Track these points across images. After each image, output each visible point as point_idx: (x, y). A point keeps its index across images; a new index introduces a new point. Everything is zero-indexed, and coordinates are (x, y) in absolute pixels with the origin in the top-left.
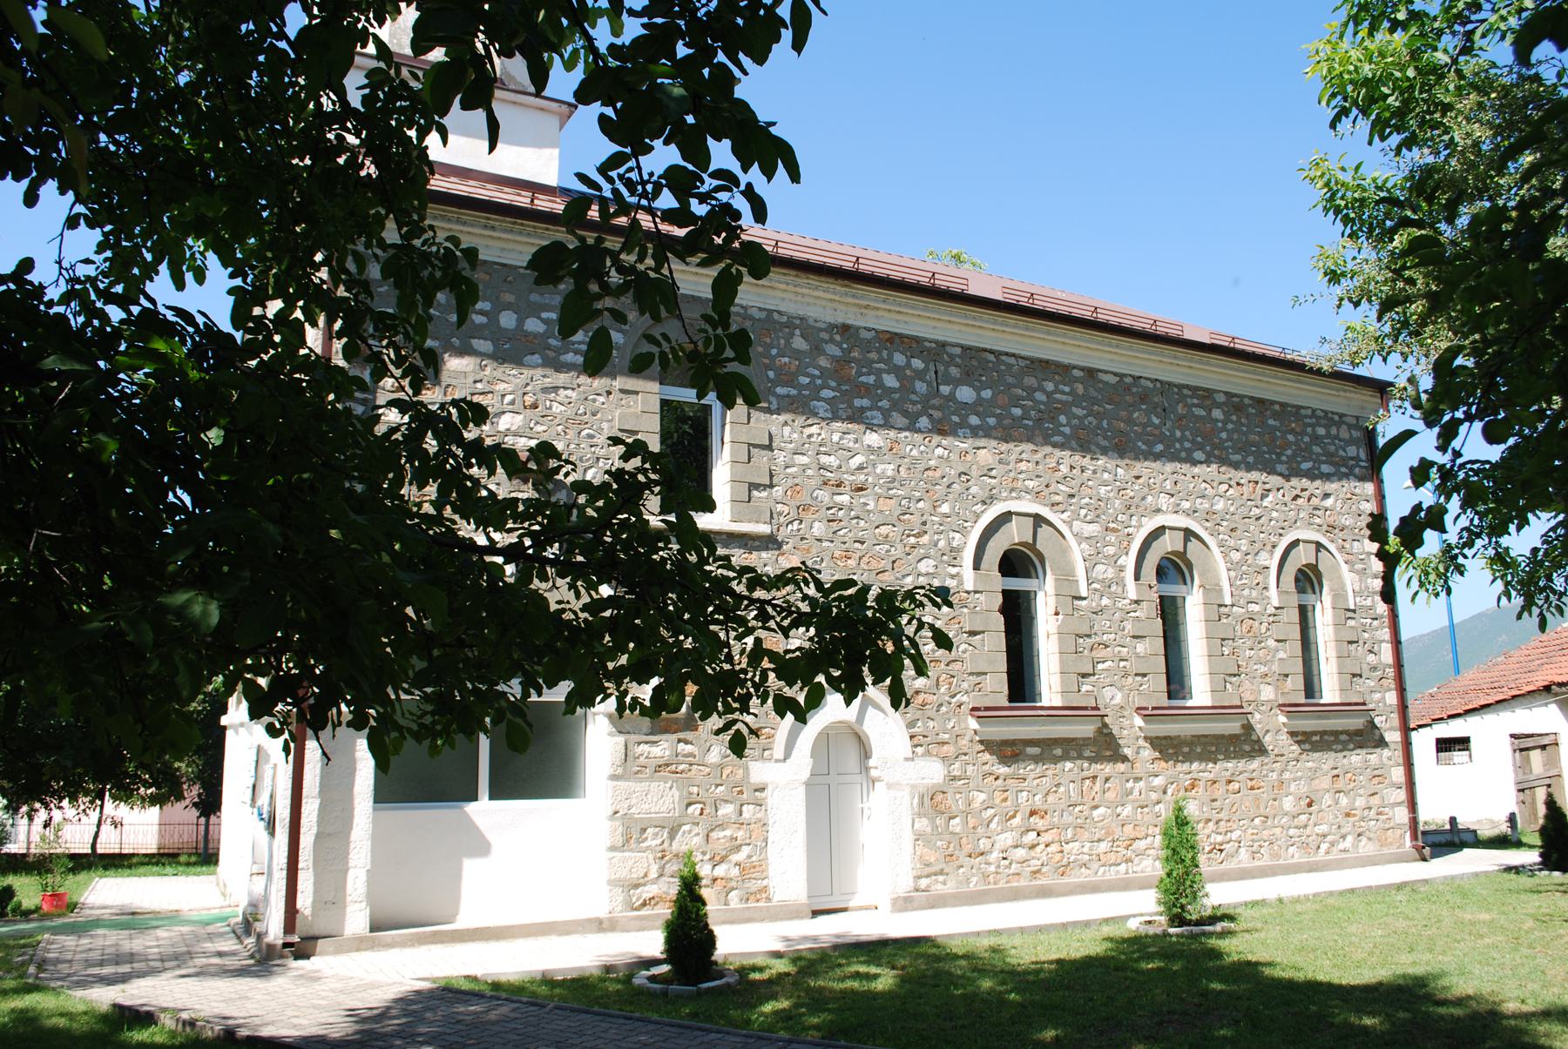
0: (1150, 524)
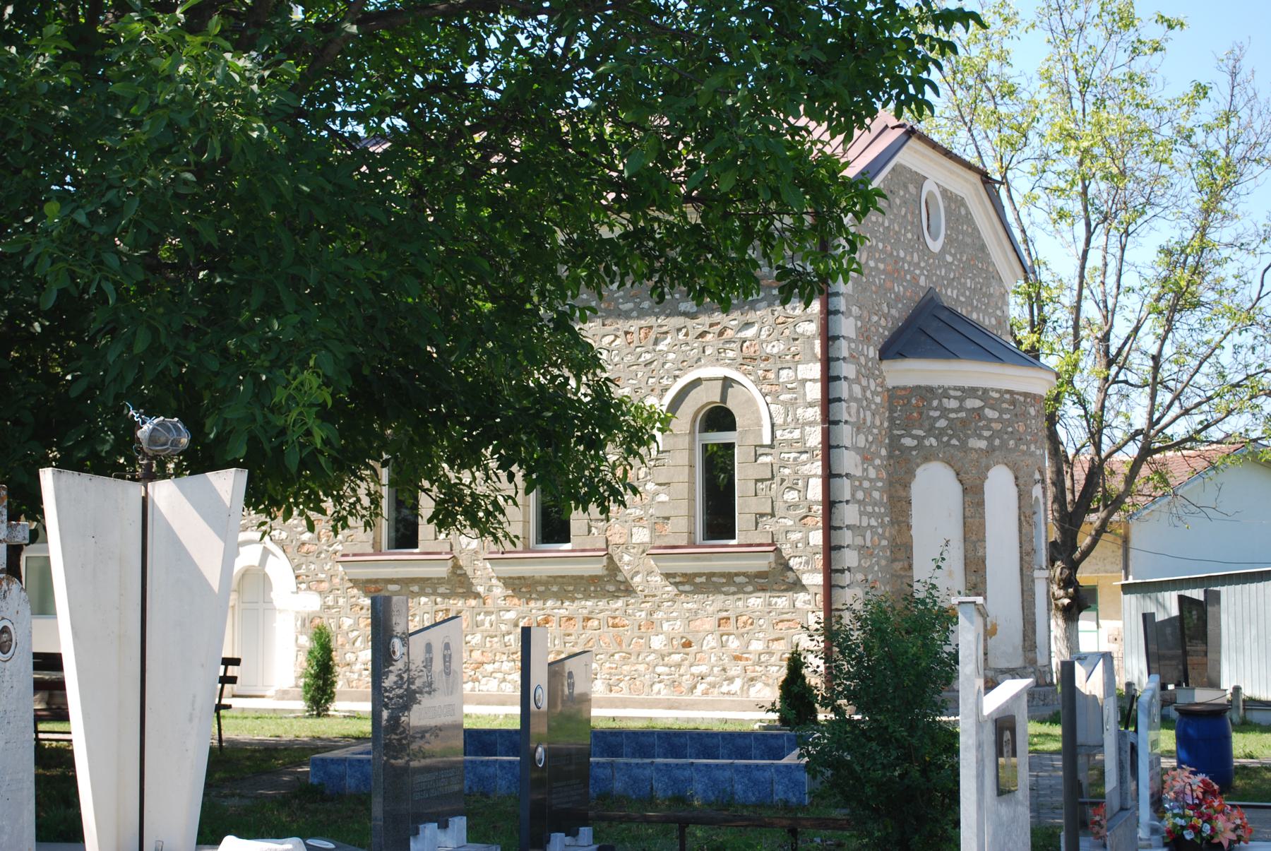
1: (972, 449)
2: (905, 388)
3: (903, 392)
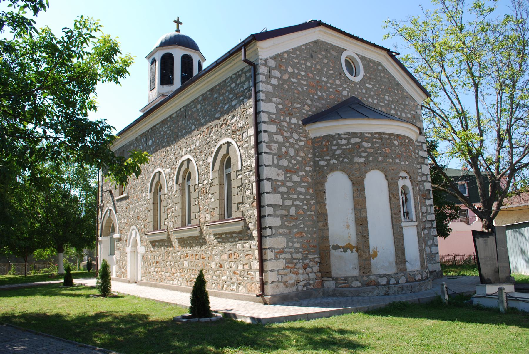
0: (180, 162)
1: (356, 163)
2: (319, 137)
3: (319, 139)
